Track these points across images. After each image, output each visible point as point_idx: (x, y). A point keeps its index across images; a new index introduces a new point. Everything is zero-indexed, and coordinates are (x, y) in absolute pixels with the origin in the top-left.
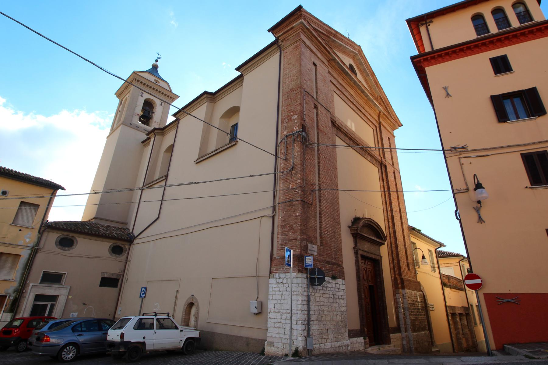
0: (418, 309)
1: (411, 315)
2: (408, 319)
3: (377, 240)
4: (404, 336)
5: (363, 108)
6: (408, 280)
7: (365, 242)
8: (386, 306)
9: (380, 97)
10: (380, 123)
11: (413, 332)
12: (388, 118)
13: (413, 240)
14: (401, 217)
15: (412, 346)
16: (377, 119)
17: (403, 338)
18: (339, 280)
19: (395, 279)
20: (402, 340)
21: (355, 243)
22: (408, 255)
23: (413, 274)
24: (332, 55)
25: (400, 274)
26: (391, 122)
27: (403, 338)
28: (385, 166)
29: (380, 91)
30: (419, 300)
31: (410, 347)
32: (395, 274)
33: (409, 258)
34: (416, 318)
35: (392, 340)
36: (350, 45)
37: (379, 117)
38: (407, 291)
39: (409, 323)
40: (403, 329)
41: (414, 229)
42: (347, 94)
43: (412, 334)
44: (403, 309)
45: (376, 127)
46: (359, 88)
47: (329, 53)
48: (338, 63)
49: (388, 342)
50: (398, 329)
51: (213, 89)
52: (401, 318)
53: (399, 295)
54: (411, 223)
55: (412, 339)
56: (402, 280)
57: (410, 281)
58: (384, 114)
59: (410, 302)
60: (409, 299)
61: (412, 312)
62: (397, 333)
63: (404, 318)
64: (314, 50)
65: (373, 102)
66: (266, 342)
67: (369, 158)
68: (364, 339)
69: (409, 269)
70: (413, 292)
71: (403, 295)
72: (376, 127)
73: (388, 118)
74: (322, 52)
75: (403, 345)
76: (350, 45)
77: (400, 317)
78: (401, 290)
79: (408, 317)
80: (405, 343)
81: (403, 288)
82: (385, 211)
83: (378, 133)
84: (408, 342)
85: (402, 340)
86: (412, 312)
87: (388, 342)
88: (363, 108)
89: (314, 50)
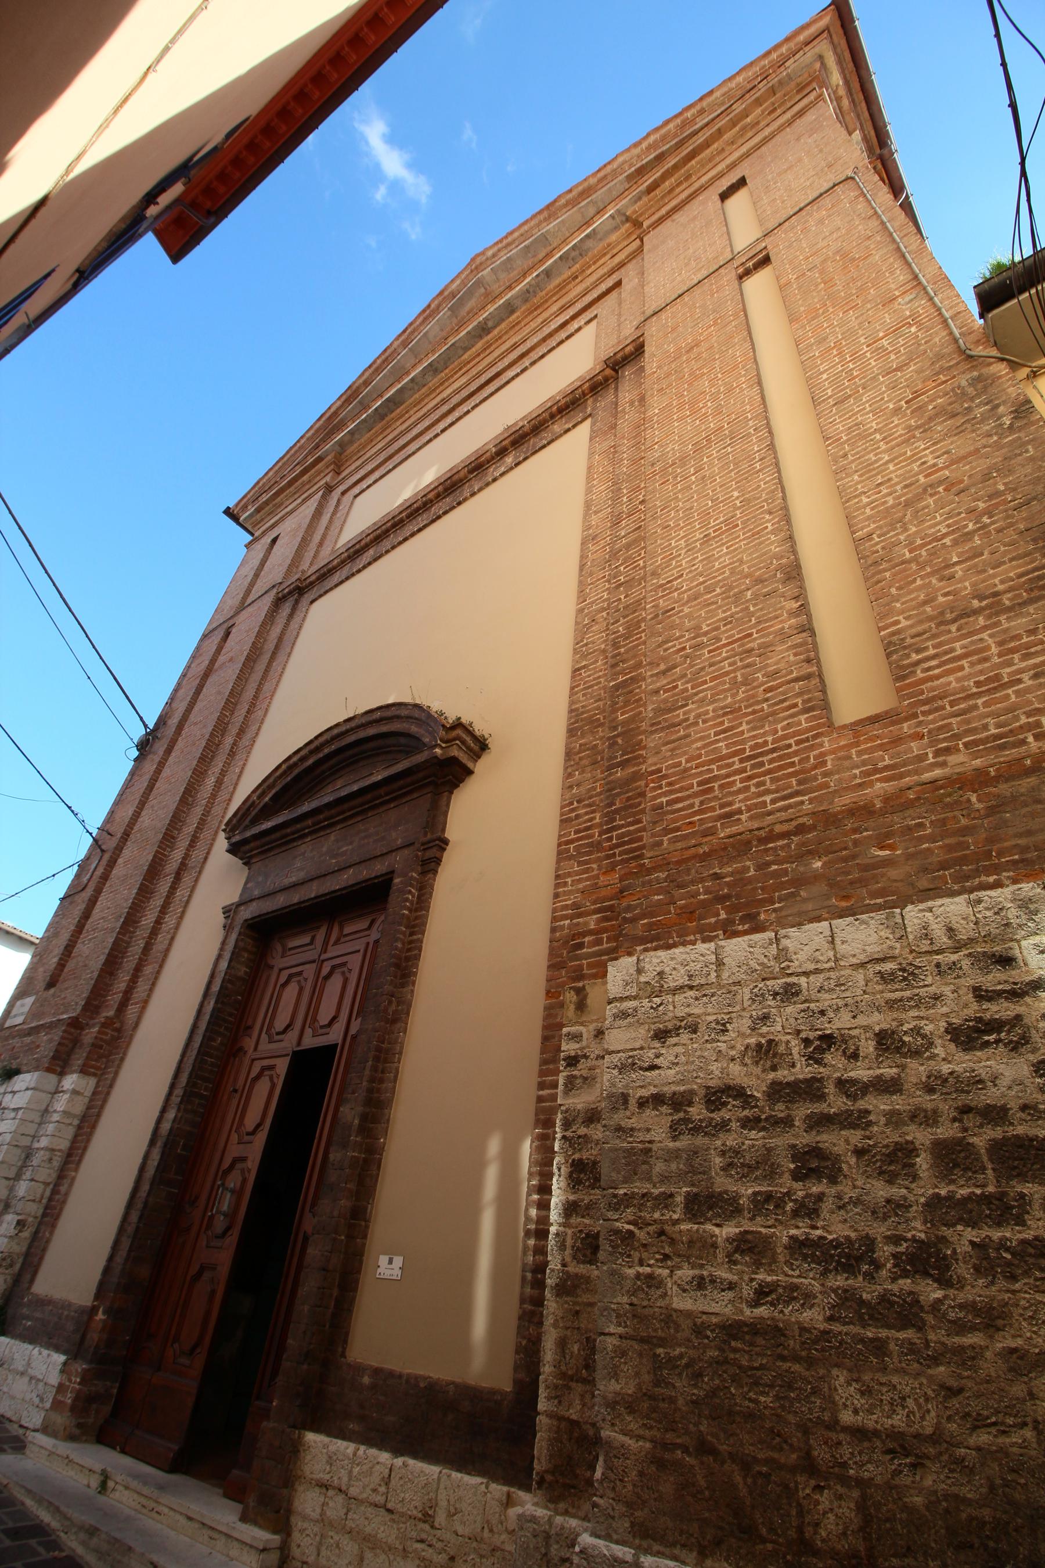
62: (463, 1463)
65: (548, 273)
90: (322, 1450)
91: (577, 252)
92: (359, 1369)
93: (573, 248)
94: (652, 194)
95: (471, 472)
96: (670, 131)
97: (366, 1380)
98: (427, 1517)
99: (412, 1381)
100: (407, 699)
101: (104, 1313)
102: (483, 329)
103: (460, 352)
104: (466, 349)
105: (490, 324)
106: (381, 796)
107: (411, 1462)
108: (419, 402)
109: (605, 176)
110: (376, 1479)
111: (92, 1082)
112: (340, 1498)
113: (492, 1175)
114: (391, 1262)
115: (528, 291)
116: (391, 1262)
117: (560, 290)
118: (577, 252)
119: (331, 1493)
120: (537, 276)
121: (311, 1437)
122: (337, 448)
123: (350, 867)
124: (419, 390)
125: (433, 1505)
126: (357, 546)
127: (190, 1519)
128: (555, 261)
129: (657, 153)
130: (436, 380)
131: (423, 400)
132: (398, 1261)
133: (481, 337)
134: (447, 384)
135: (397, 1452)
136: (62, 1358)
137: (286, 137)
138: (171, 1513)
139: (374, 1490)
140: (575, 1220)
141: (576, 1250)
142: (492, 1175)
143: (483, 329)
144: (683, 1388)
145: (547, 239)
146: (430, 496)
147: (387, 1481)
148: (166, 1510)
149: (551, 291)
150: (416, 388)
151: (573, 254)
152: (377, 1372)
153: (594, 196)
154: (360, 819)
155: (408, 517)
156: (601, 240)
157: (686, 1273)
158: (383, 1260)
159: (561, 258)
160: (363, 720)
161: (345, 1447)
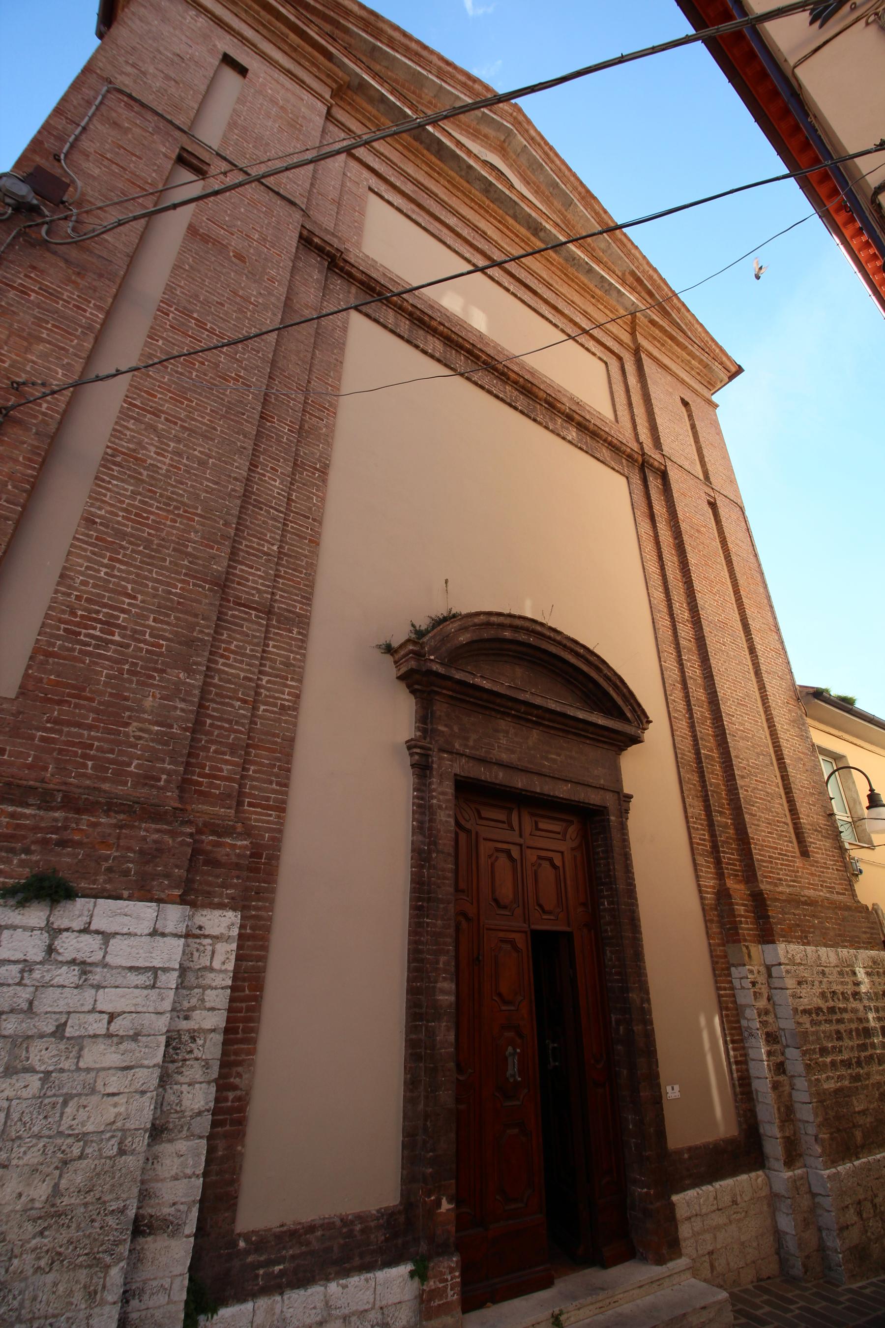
0: (867, 1032)
1: (822, 1067)
2: (802, 1093)
3: (601, 721)
4: (780, 1188)
5: (549, 286)
6: (795, 901)
7: (503, 724)
8: (649, 1036)
9: (633, 273)
10: (637, 352)
11: (834, 1163)
12: (672, 338)
13: (821, 738)
14: (752, 650)
15: (834, 1242)
16: (626, 337)
17: (773, 1199)
18: (107, 913)
19: (723, 894)
20: (773, 1211)
21: (425, 719)
22: (797, 795)
23: (832, 874)
24: (341, 66)
25: (749, 872)
26: (694, 357)
27: (773, 1199)
28: (664, 475)
29: (629, 254)
30: (863, 989)
31: (822, 1248)
32: (720, 875)
33: (803, 809)
34: (856, 1078)
35: (685, 1231)
36: (464, 85)
37: (633, 334)
38: (783, 950)
39: (806, 1113)
40: (774, 1148)
41: (819, 694)
42: (452, 221)
43: (826, 1174)
44: (771, 1038)
45: (620, 359)
46: (500, 199)
47: (329, 56)
48: (383, 99)
49: (664, 1244)
50: (744, 1151)
51: (859, 705)
52: (763, 1086)
53: (743, 971)
54: (806, 676)
55: (827, 1202)
56: (759, 902)
57: (811, 902)
58: (653, 322)
59: (810, 998)
60: (804, 991)
61: (824, 1051)
62: (734, 1173)
63: (776, 1086)
64: (249, 33)
65: (590, 270)
66: (461, 1078)
67: (572, 433)
68: (420, 1274)
69: (805, 853)
70: (828, 955)
71: (769, 968)
72: (620, 359)
73: (672, 338)
74: (278, 41)
75: (778, 1234)
76: (464, 85)
77: (756, 1084)
78: (756, 950)
79: (801, 1083)
80: (786, 1223)
81: (767, 936)
82: (664, 622)
83: (633, 380)
84: (810, 1219)
85: (773, 1211)
86: (824, 1051)
87: (664, 1244)
88: (549, 286)
89: (249, 33)
90: (686, 1201)
91: (608, 288)
92: (679, 1152)
93: (611, 284)
94: (650, 325)
95: (546, 402)
96: (663, 290)
97: (686, 1156)
98: (735, 1202)
99: (706, 1146)
100: (540, 619)
101: (449, 1202)
102: (536, 229)
103: (511, 212)
104: (515, 217)
105: (542, 234)
106: (587, 731)
107: (722, 1183)
108: (454, 186)
109: (625, 245)
110: (711, 1199)
111: (222, 922)
112: (699, 1218)
113: (705, 1035)
114: (673, 1089)
115: (574, 259)
116: (673, 1089)
117: (583, 289)
118: (608, 288)
119: (693, 1219)
120: (587, 263)
121: (675, 1198)
122: (356, 82)
123: (571, 781)
124: (461, 177)
125: (735, 1195)
126: (426, 318)
127: (640, 1287)
128: (599, 274)
129: (653, 291)
130: (477, 193)
131: (458, 189)
132: (677, 1087)
133: (529, 228)
134: (482, 212)
135: (710, 1183)
136: (404, 1270)
137: (728, 53)
138: (626, 1294)
139: (712, 1205)
140: (772, 1058)
141: (775, 1070)
142: (705, 1035)
143: (536, 229)
144: (832, 1114)
145: (570, 206)
146: (513, 375)
147: (716, 1198)
148: (622, 1295)
149: (579, 280)
150: (463, 173)
151: (606, 285)
152: (690, 1149)
153: (613, 245)
154: (561, 734)
155: (485, 363)
156: (618, 301)
157: (824, 1076)
158: (669, 1089)
159: (602, 277)
160: (565, 642)
161: (691, 1193)
